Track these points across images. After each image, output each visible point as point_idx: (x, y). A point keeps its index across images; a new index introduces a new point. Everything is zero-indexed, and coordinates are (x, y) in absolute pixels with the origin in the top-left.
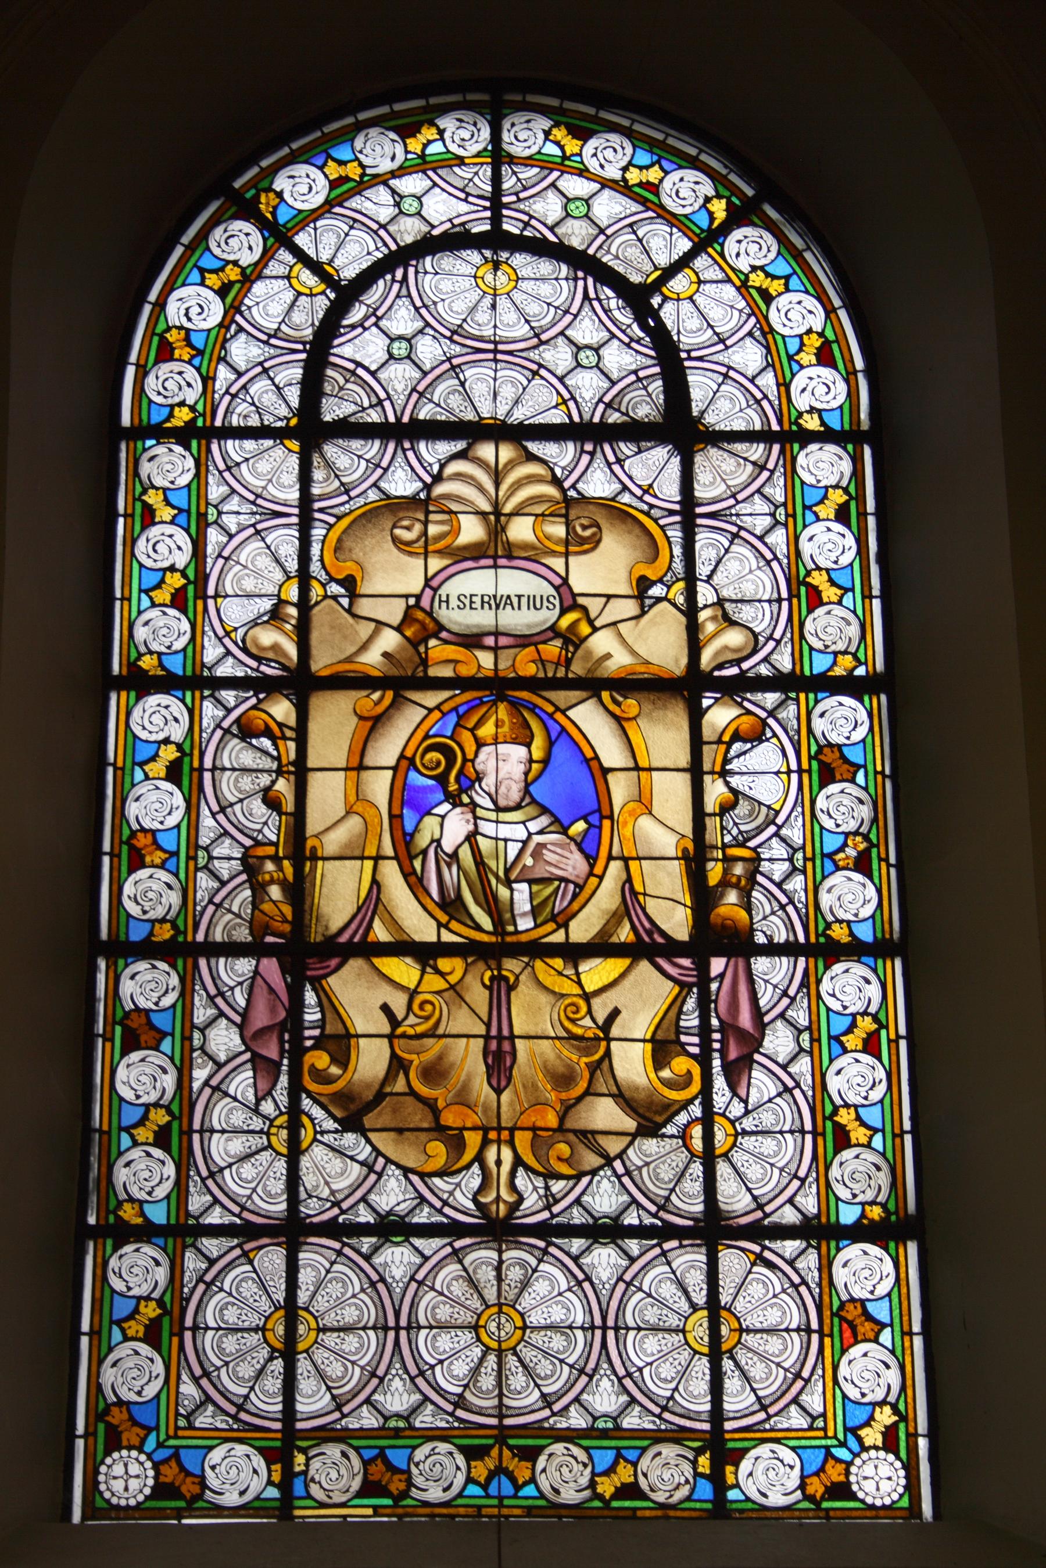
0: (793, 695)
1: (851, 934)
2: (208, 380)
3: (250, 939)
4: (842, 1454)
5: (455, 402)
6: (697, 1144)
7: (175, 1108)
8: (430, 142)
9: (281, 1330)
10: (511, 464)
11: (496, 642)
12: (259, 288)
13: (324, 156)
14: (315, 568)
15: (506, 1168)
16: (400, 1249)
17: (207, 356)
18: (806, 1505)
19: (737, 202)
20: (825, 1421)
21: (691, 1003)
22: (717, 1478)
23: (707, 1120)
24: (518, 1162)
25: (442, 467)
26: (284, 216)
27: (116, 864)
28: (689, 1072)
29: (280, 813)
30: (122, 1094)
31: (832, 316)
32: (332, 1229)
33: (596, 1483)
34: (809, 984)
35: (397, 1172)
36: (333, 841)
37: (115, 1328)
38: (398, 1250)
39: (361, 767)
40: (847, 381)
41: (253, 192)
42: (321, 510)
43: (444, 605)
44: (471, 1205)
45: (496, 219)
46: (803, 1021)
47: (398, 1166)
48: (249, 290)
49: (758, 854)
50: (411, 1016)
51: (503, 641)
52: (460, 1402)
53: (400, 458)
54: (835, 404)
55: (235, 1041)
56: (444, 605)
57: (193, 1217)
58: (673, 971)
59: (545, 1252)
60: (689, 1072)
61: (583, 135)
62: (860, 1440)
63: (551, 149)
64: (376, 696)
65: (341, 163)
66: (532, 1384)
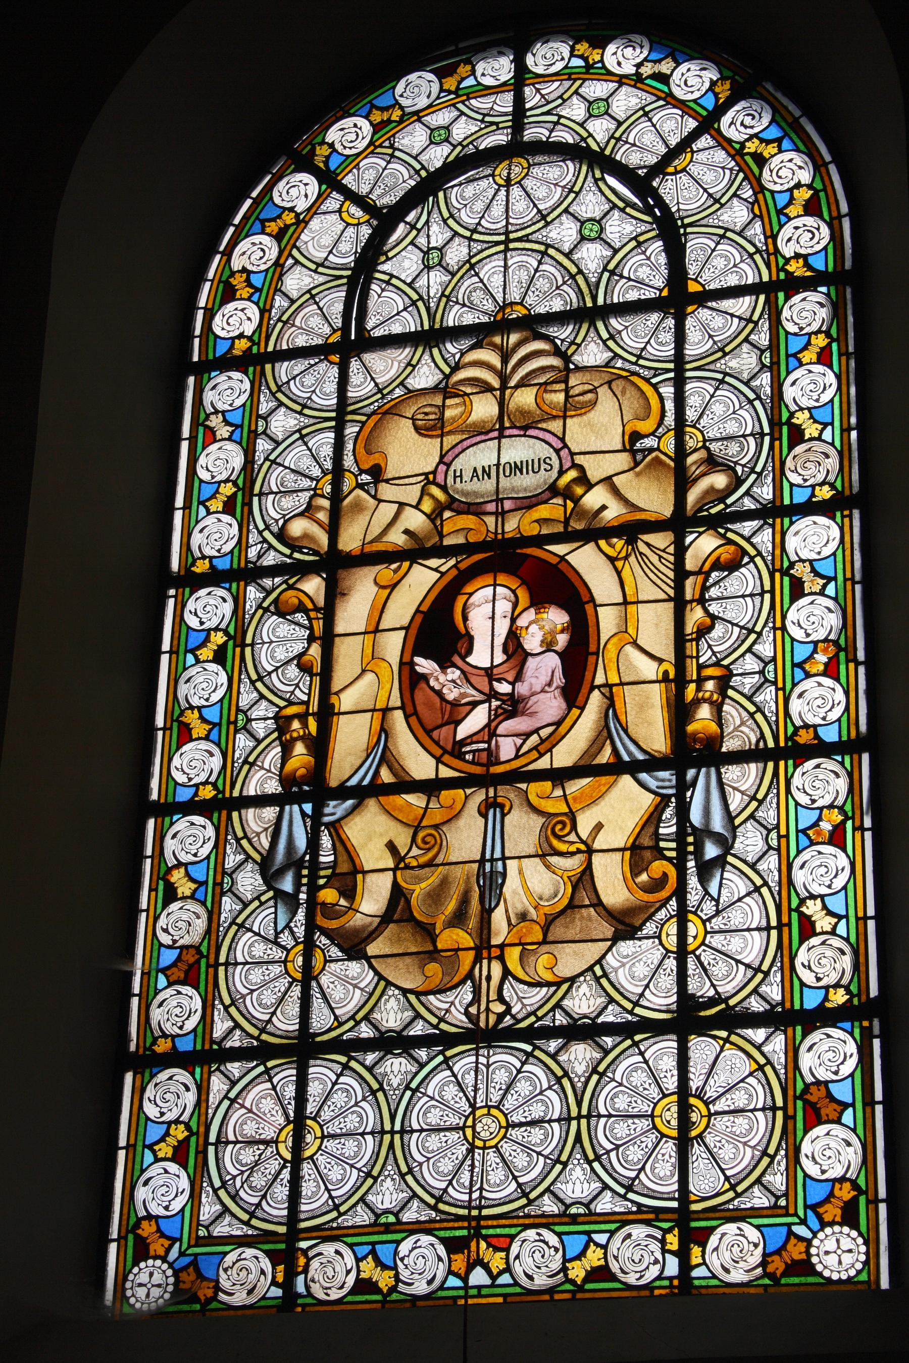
0: (770, 521)
4: (801, 1231)
6: (672, 942)
8: (463, 79)
12: (315, 223)
14: (348, 461)
19: (741, 81)
20: (787, 1200)
21: (669, 813)
24: (506, 973)
28: (665, 875)
29: (312, 675)
31: (823, 169)
33: (567, 1269)
35: (397, 992)
38: (396, 1061)
39: (377, 630)
40: (830, 225)
42: (354, 412)
43: (458, 480)
44: (464, 1018)
49: (731, 671)
50: (414, 848)
56: (458, 480)
57: (216, 1043)
58: (652, 784)
60: (665, 875)
61: (601, 44)
63: (577, 62)
64: (394, 566)
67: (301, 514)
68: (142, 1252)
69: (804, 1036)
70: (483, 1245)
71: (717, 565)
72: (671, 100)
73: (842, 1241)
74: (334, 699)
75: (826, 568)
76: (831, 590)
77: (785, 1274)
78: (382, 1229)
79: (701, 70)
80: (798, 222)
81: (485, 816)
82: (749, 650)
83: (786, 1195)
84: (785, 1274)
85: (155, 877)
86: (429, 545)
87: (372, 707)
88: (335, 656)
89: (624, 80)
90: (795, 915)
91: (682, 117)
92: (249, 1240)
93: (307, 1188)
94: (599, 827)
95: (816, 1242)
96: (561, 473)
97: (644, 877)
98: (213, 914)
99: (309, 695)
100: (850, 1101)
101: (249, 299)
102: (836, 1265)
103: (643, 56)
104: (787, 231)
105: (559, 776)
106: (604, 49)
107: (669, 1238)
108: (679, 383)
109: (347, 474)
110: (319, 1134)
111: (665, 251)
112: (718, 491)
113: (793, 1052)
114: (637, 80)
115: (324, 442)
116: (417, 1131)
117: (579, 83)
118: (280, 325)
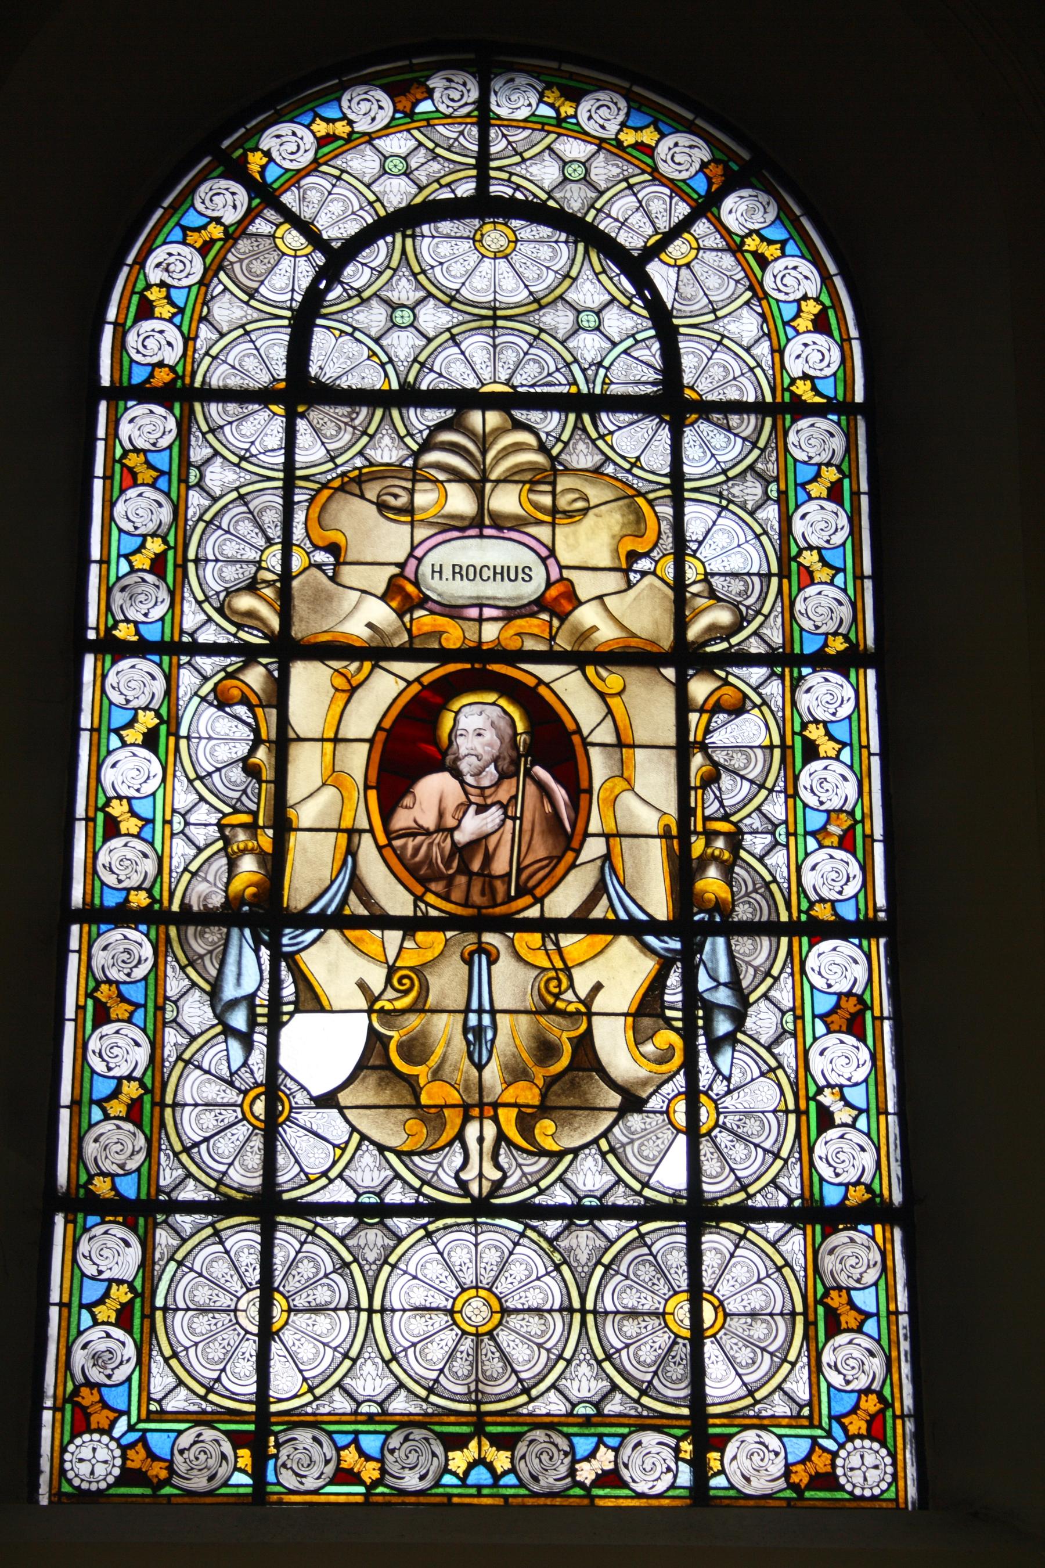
0: (778, 670)
1: (835, 913)
2: (189, 339)
7: (148, 1081)
9: (276, 1311)
10: (499, 432)
13: (311, 115)
14: (298, 533)
15: (488, 1144)
16: (585, 1233)
17: (196, 317)
18: (789, 1494)
19: (735, 168)
21: (674, 979)
26: (272, 174)
28: (672, 1047)
29: (260, 782)
38: (583, 1234)
41: (240, 151)
44: (453, 1183)
45: (483, 180)
46: (787, 1002)
47: (372, 1142)
54: (828, 372)
55: (207, 1015)
59: (743, 1237)
60: (672, 1047)
61: (575, 97)
63: (545, 111)
65: (328, 121)
68: (82, 1425)
69: (825, 1237)
70: (486, 1443)
73: (861, 1480)
74: (291, 813)
77: (810, 1487)
79: (691, 147)
81: (469, 963)
83: (810, 1404)
84: (810, 1487)
86: (397, 643)
87: (336, 826)
88: (291, 758)
91: (671, 198)
94: (598, 987)
97: (648, 1048)
98: (156, 1045)
99: (258, 804)
100: (874, 1310)
101: (170, 320)
105: (549, 927)
108: (678, 503)
110: (285, 1307)
112: (722, 628)
117: (553, 136)
118: (208, 360)
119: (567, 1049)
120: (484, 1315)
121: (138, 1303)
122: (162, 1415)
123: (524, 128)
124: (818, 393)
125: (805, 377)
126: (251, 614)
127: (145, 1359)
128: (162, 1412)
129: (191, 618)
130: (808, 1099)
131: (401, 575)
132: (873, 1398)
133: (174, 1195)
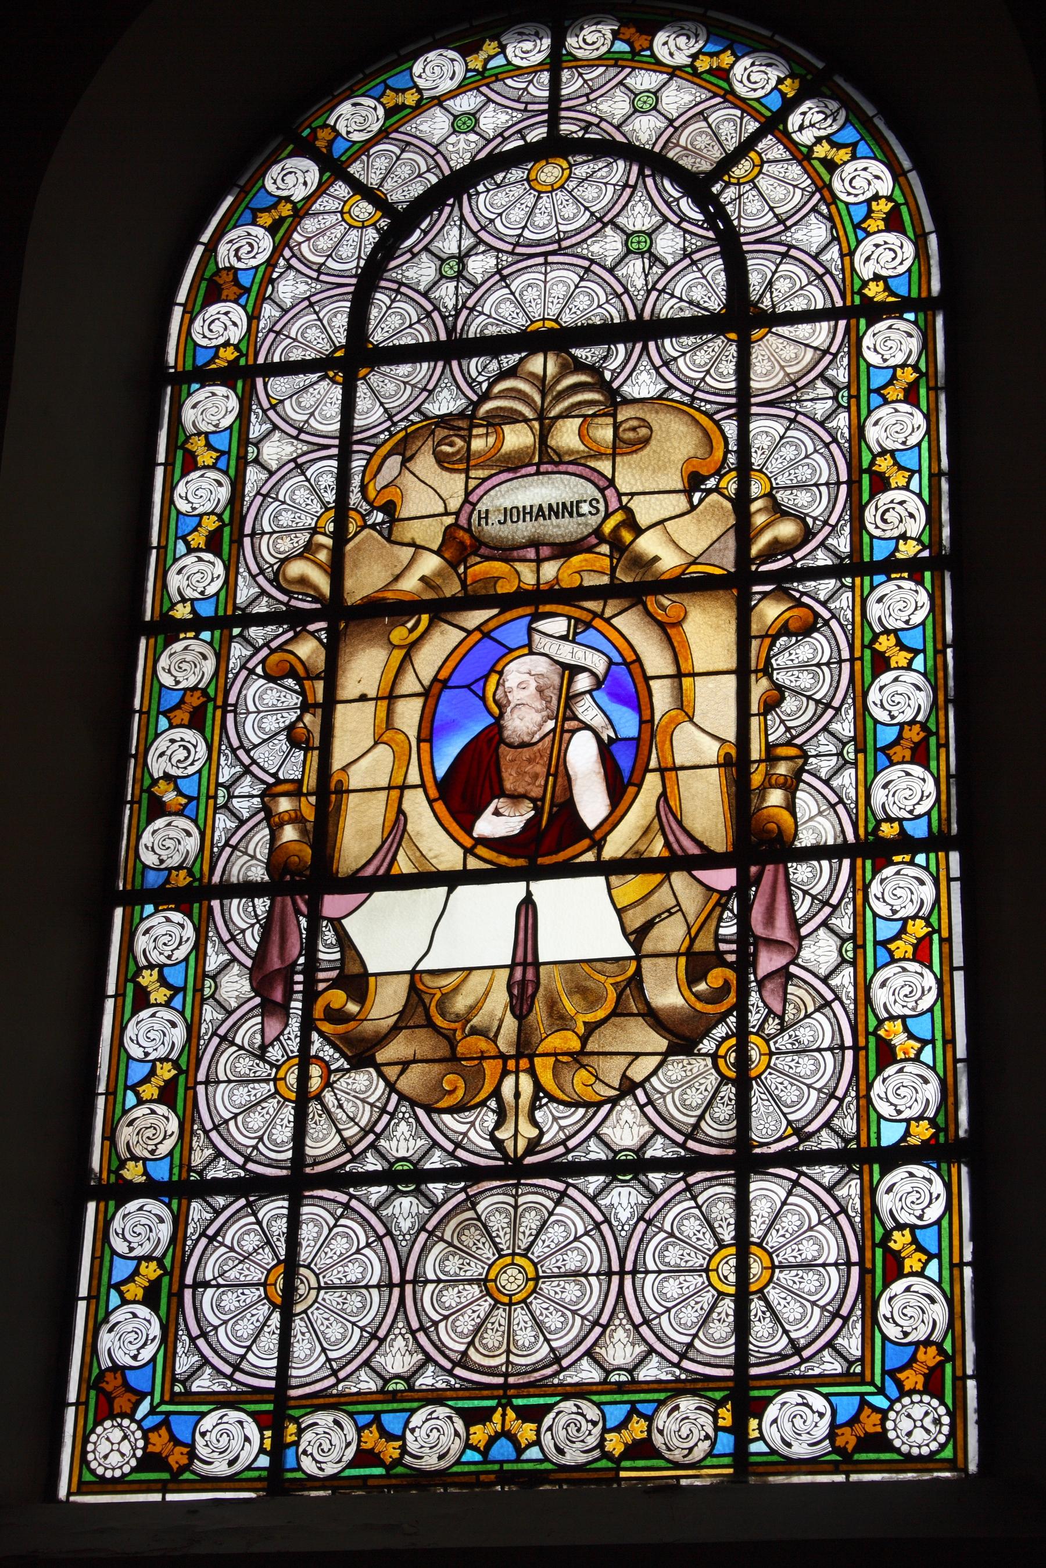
2: (253, 317)
3: (266, 878)
5: (507, 310)
8: (491, 58)
11: (537, 553)
12: (310, 225)
17: (253, 294)
22: (738, 1429)
23: (742, 1033)
25: (491, 386)
27: (162, 557)
28: (726, 982)
30: (132, 1054)
31: (902, 179)
32: (338, 1180)
34: (859, 889)
36: (356, 779)
37: (113, 1292)
42: (360, 442)
44: (489, 1146)
45: (553, 123)
48: (299, 223)
51: (545, 551)
52: (463, 1360)
53: (447, 380)
56: (483, 522)
59: (796, 1183)
62: (899, 1384)
63: (621, 46)
66: (542, 1339)
67: (300, 556)
68: (106, 1411)
70: (511, 1414)
71: (785, 630)
72: (730, 97)
75: (913, 639)
76: (918, 663)
77: (858, 1449)
78: (389, 1397)
79: (769, 65)
80: (879, 238)
82: (825, 729)
83: (861, 1360)
84: (858, 1449)
85: (122, 978)
89: (678, 72)
90: (872, 1040)
92: (231, 1398)
93: (301, 1348)
95: (892, 1415)
96: (608, 515)
97: (702, 987)
102: (926, 1436)
103: (698, 46)
104: (866, 247)
106: (654, 36)
107: (722, 1412)
108: (744, 419)
109: (352, 514)
111: (725, 270)
113: (869, 1193)
114: (689, 73)
115: (324, 473)
116: (432, 1281)
119: (612, 995)
120: (519, 1282)
121: (166, 1280)
122: (189, 1397)
123: (598, 66)
124: (892, 294)
125: (877, 277)
126: (303, 581)
127: (171, 1338)
128: (188, 1393)
129: (244, 593)
130: (868, 1033)
131: (456, 525)
132: (932, 1350)
133: (391, 1189)
